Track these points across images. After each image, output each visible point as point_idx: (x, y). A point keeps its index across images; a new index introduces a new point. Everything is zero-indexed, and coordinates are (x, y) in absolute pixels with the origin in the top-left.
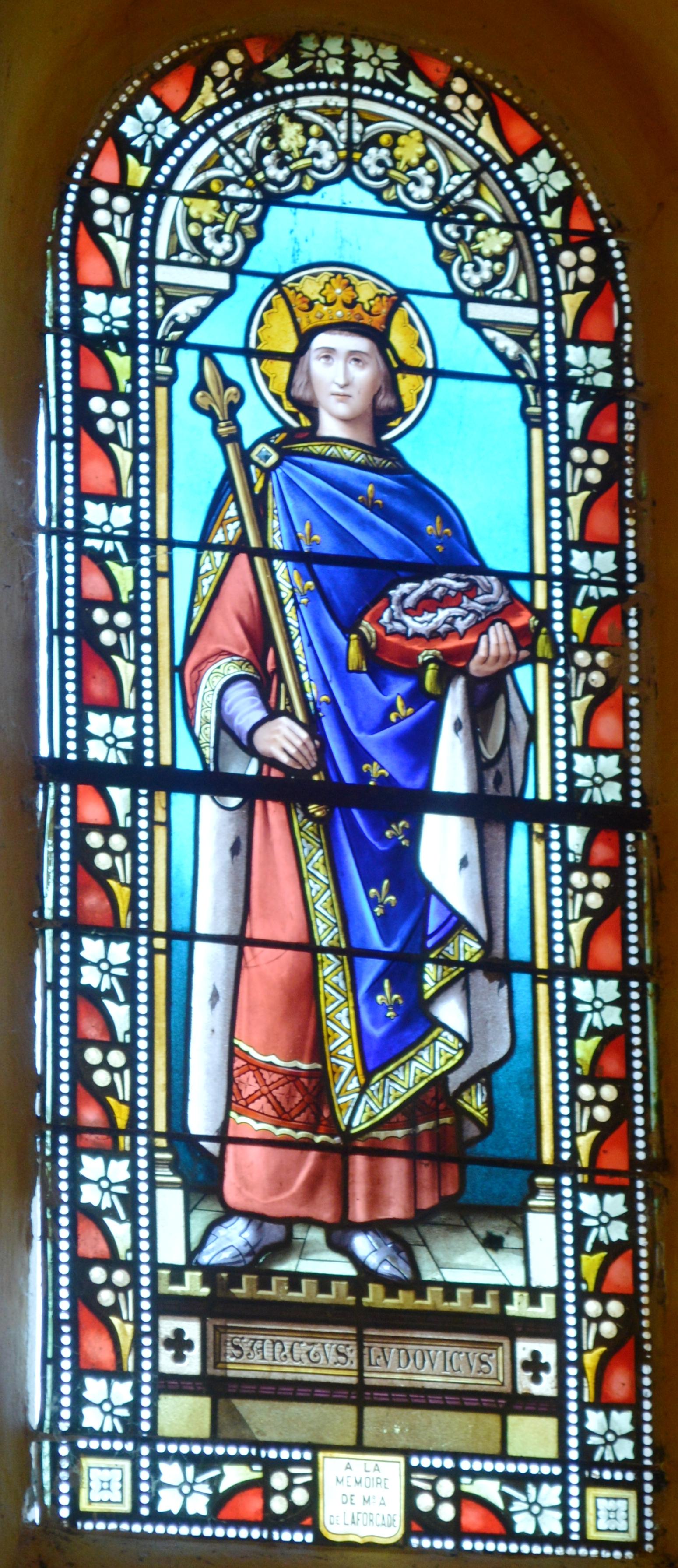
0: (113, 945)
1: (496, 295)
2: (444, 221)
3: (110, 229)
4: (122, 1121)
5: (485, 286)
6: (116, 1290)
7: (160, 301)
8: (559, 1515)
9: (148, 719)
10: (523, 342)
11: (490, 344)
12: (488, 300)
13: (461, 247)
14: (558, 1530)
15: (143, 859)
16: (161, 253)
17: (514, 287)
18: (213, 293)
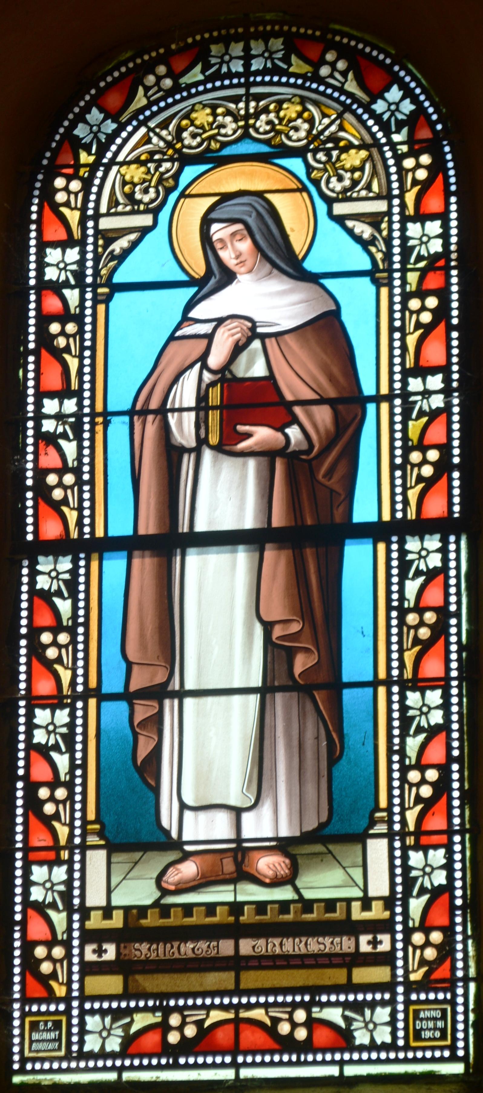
0: (58, 712)
1: (355, 195)
2: (315, 151)
3: (67, 204)
4: (63, 841)
5: (345, 190)
6: (54, 961)
7: (101, 242)
8: (388, 1029)
9: (77, 866)
10: (376, 225)
11: (350, 232)
12: (350, 199)
13: (328, 167)
14: (388, 1040)
15: (78, 806)
16: (103, 209)
17: (368, 187)
18: (141, 229)
